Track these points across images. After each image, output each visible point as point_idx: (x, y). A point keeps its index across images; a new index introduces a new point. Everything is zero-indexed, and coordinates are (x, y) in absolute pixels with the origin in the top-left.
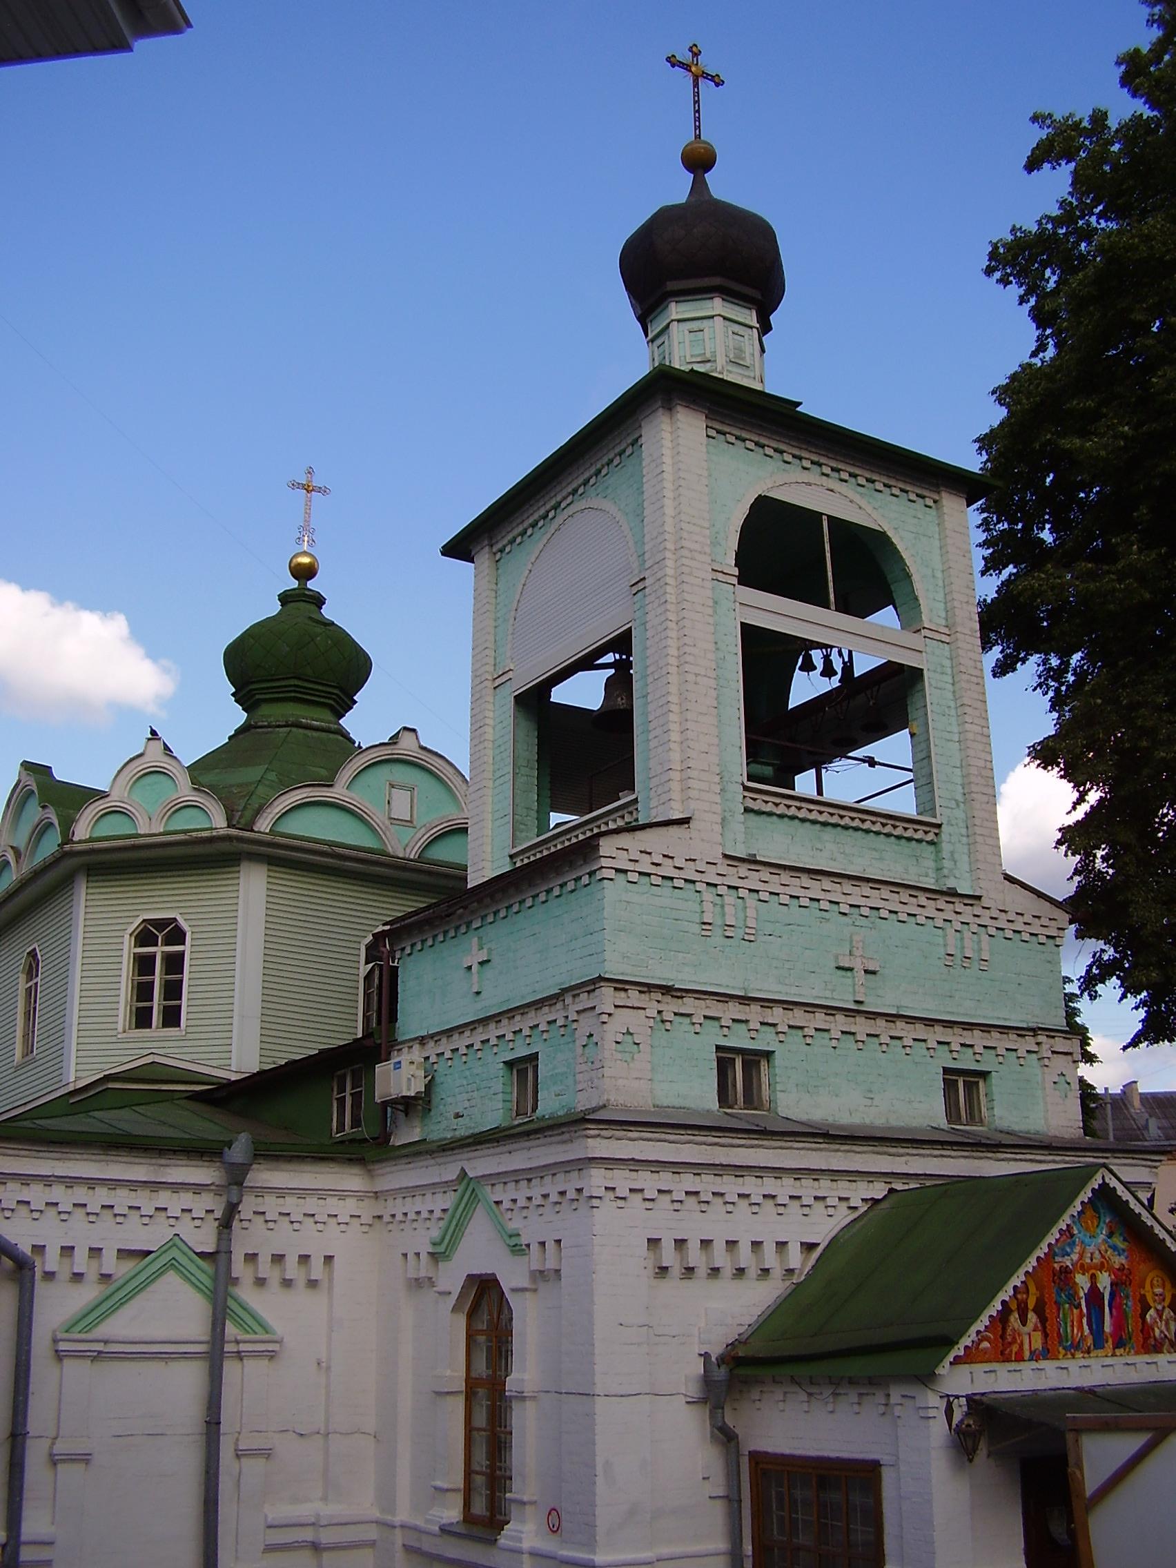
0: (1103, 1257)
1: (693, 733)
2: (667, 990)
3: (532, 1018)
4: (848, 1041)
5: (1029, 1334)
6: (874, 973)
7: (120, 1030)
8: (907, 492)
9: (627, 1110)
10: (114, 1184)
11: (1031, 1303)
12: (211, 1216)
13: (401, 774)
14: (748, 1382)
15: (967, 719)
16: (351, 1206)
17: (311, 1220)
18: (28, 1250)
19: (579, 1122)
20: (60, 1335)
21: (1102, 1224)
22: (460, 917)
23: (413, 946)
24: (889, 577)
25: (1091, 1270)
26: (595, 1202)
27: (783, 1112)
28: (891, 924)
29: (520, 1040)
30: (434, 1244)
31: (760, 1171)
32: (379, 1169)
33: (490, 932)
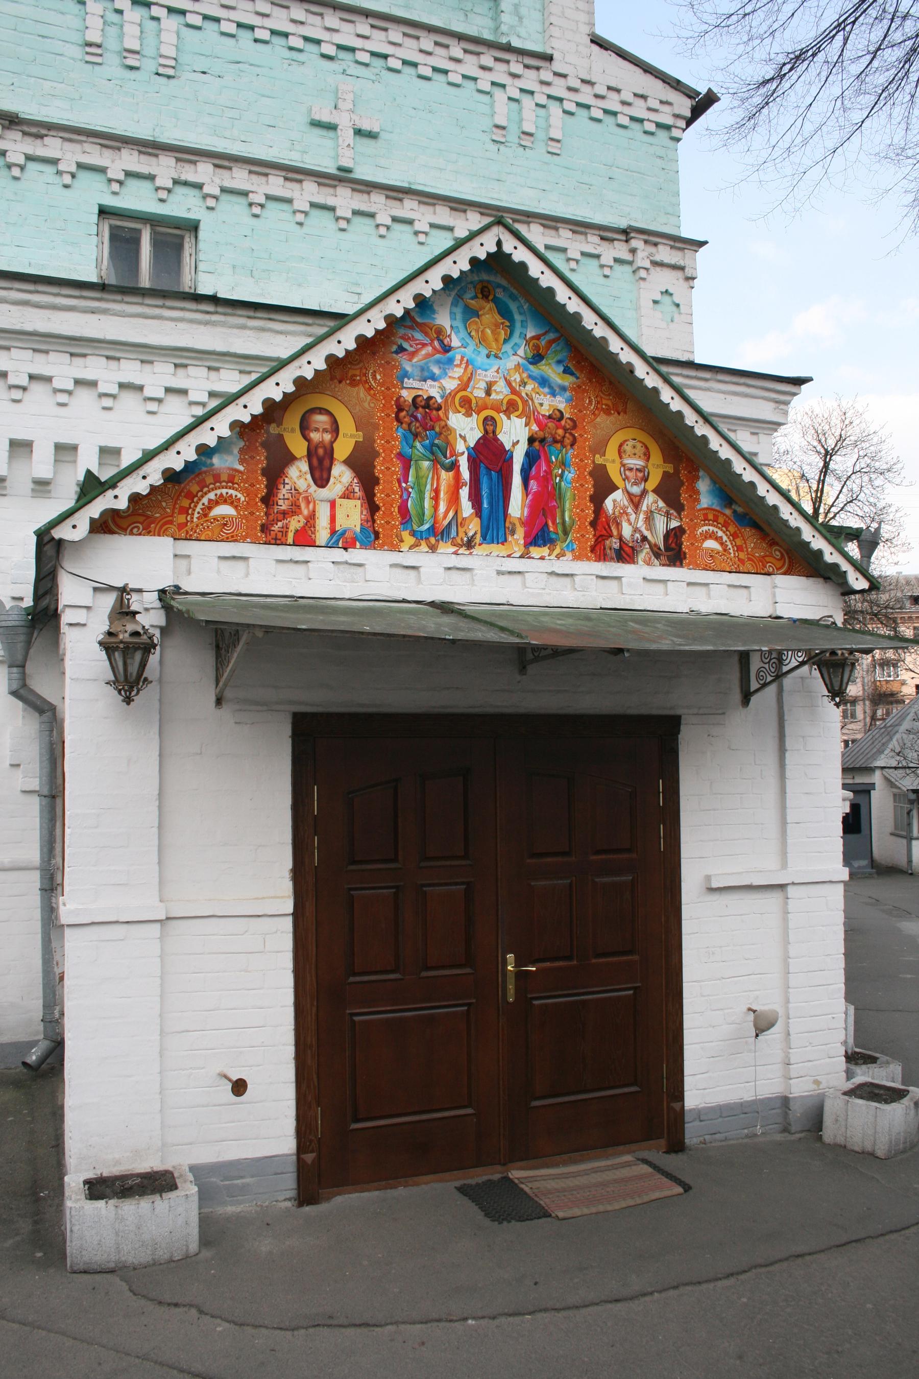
0: (513, 391)
5: (336, 501)
6: (371, 135)
11: (343, 448)
21: (516, 339)
31: (113, 350)
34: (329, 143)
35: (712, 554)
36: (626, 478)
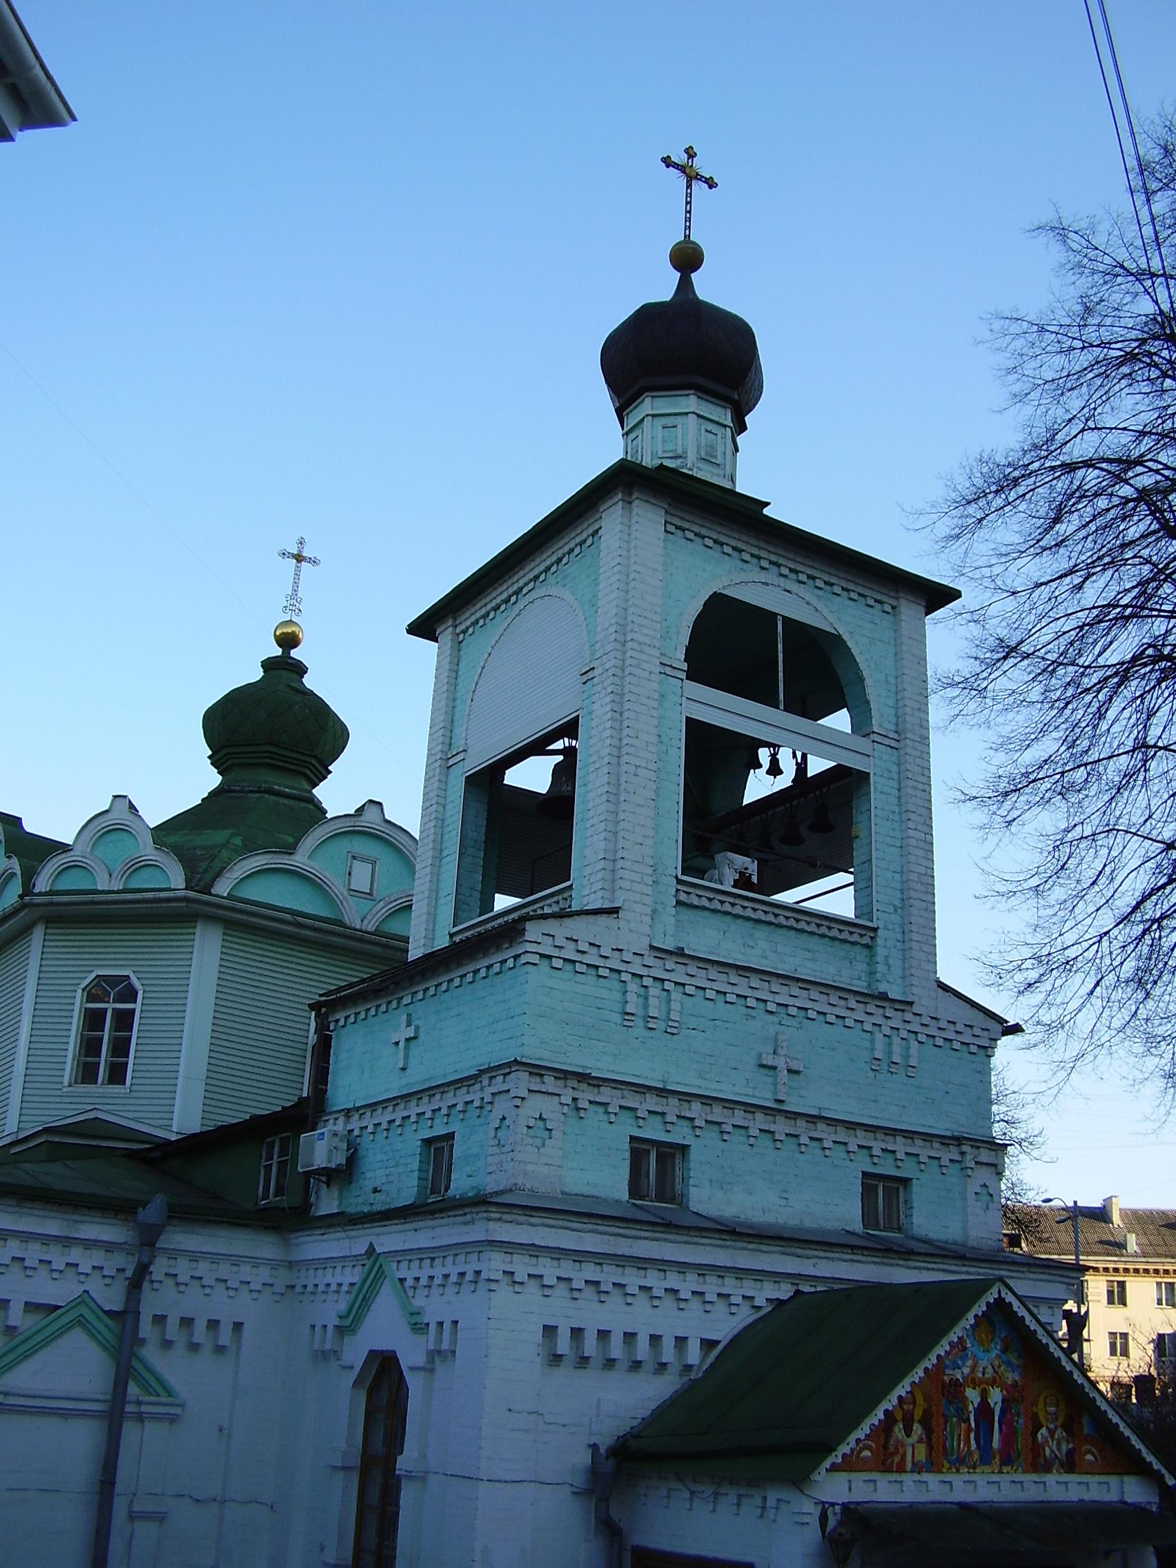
0: (995, 1372)
2: (583, 1077)
5: (914, 1446)
6: (797, 1072)
7: (66, 1083)
8: (865, 596)
9: (533, 1193)
11: (918, 1414)
12: (121, 1276)
13: (360, 846)
15: (911, 824)
16: (264, 1273)
17: (223, 1285)
19: (481, 1202)
25: (983, 1386)
26: (493, 1286)
27: (694, 1206)
28: (817, 1028)
30: (340, 1317)
31: (663, 1265)
33: (419, 1009)
34: (770, 1080)
35: (1090, 1462)
36: (1047, 1420)
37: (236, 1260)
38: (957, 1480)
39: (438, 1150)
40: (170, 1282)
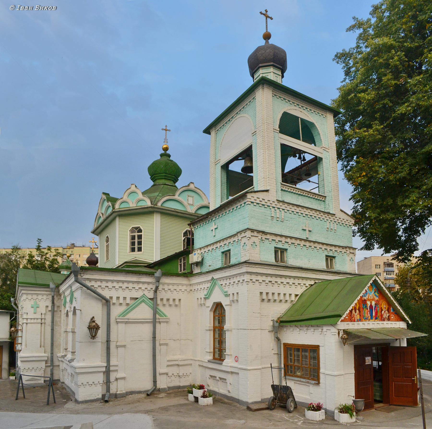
1: (266, 172)
2: (263, 232)
3: (229, 240)
4: (305, 247)
5: (356, 315)
10: (128, 282)
11: (357, 308)
12: (152, 290)
14: (282, 326)
16: (184, 288)
18: (108, 298)
20: (117, 318)
22: (210, 218)
23: (198, 226)
24: (314, 135)
25: (371, 300)
29: (226, 246)
31: (286, 277)
32: (191, 278)
33: (217, 221)
35: (392, 319)
37: (178, 285)
38: (366, 323)
39: (227, 254)
40: (163, 291)
